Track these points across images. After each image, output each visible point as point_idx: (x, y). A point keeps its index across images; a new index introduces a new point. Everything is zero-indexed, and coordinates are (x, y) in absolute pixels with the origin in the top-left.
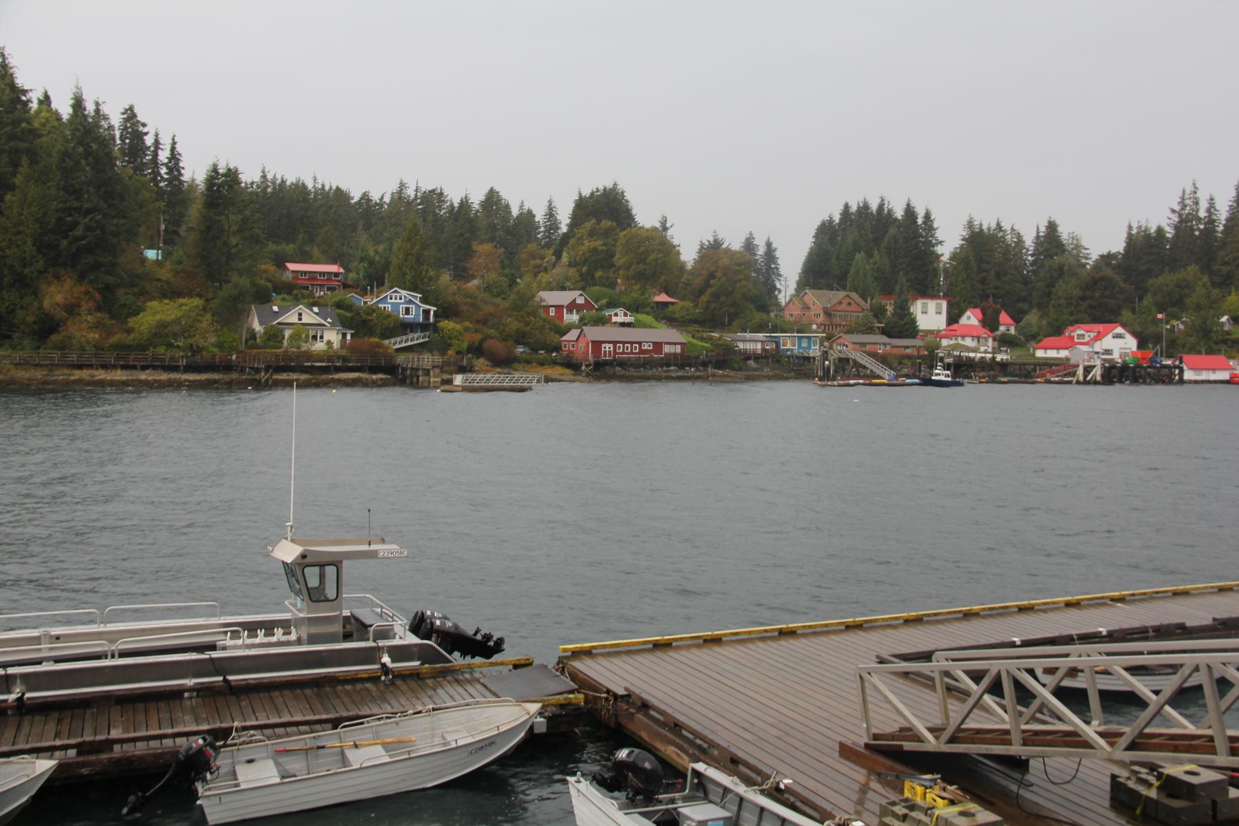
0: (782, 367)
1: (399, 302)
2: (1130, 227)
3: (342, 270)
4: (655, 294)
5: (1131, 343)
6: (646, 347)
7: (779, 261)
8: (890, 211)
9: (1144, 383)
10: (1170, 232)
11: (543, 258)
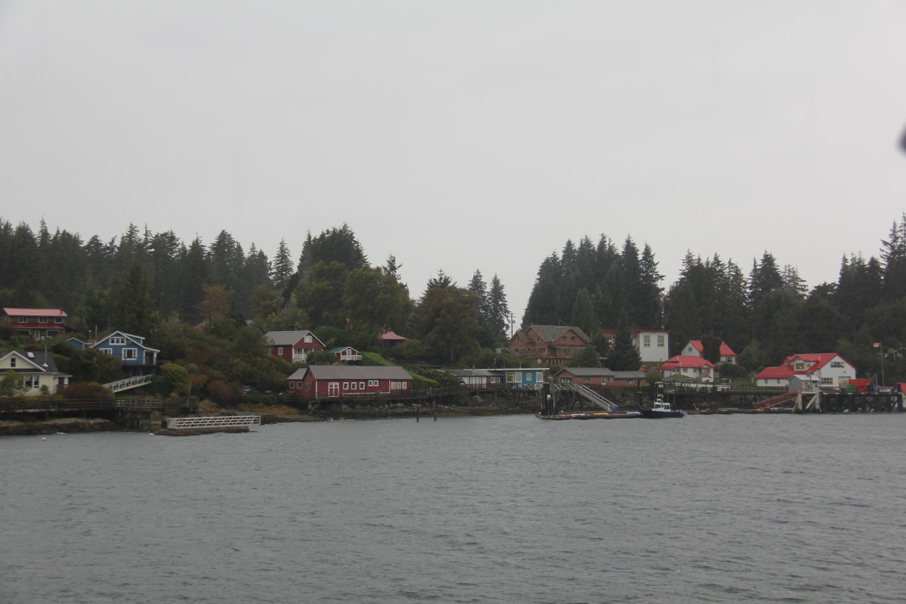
0: (506, 401)
1: (119, 344)
2: (845, 260)
3: (64, 314)
4: (382, 333)
5: (850, 372)
6: (372, 384)
7: (506, 298)
8: (611, 248)
9: (864, 411)
10: (883, 264)
11: (272, 299)
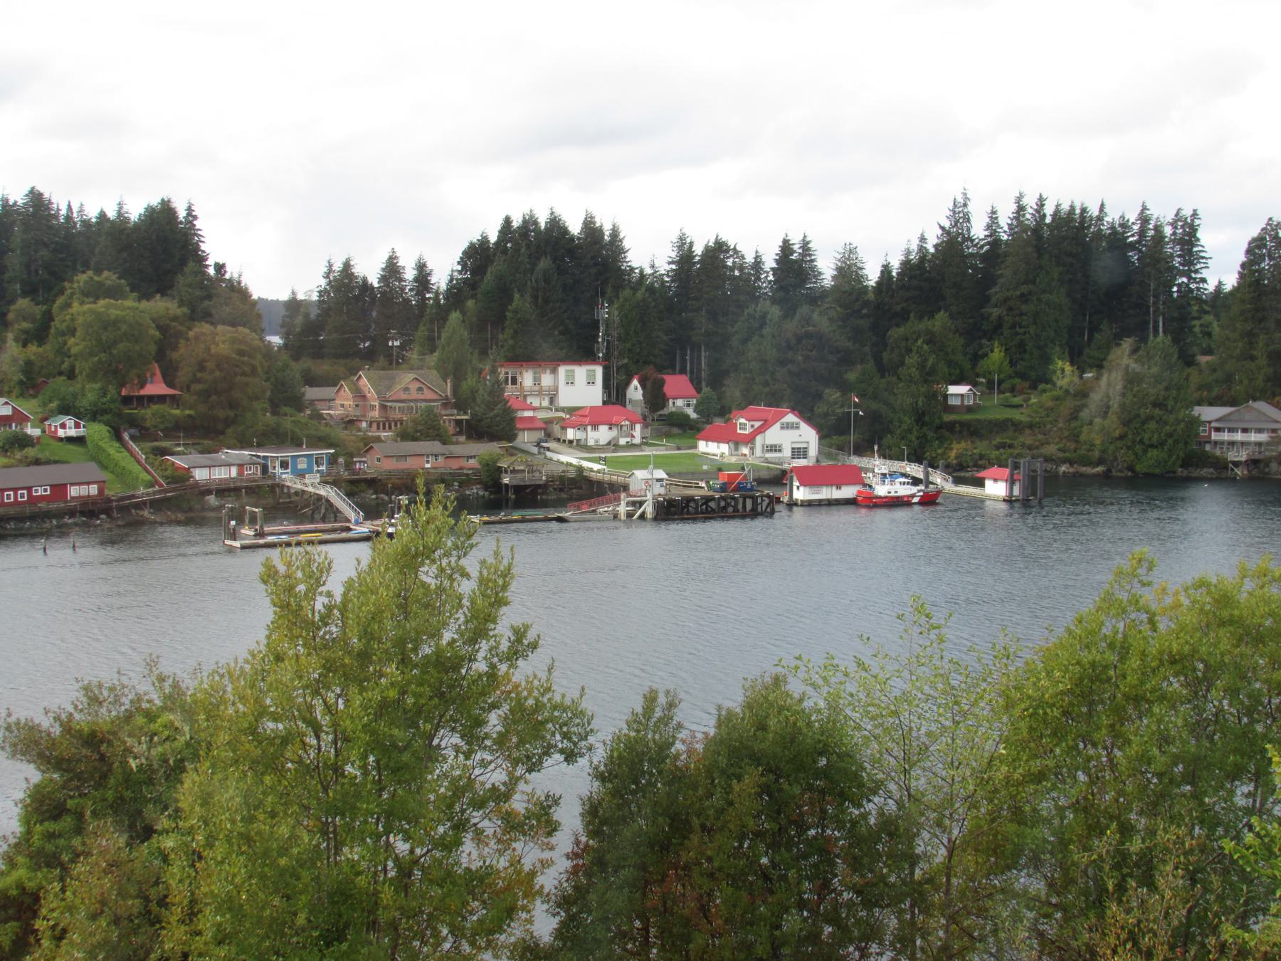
5: (808, 436)
6: (40, 492)
